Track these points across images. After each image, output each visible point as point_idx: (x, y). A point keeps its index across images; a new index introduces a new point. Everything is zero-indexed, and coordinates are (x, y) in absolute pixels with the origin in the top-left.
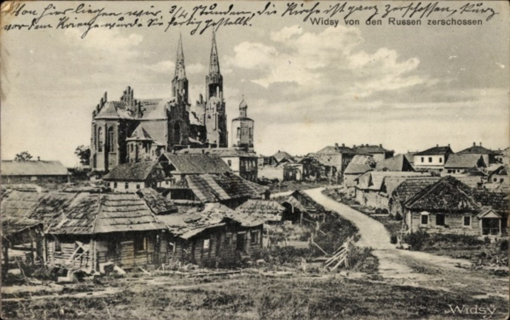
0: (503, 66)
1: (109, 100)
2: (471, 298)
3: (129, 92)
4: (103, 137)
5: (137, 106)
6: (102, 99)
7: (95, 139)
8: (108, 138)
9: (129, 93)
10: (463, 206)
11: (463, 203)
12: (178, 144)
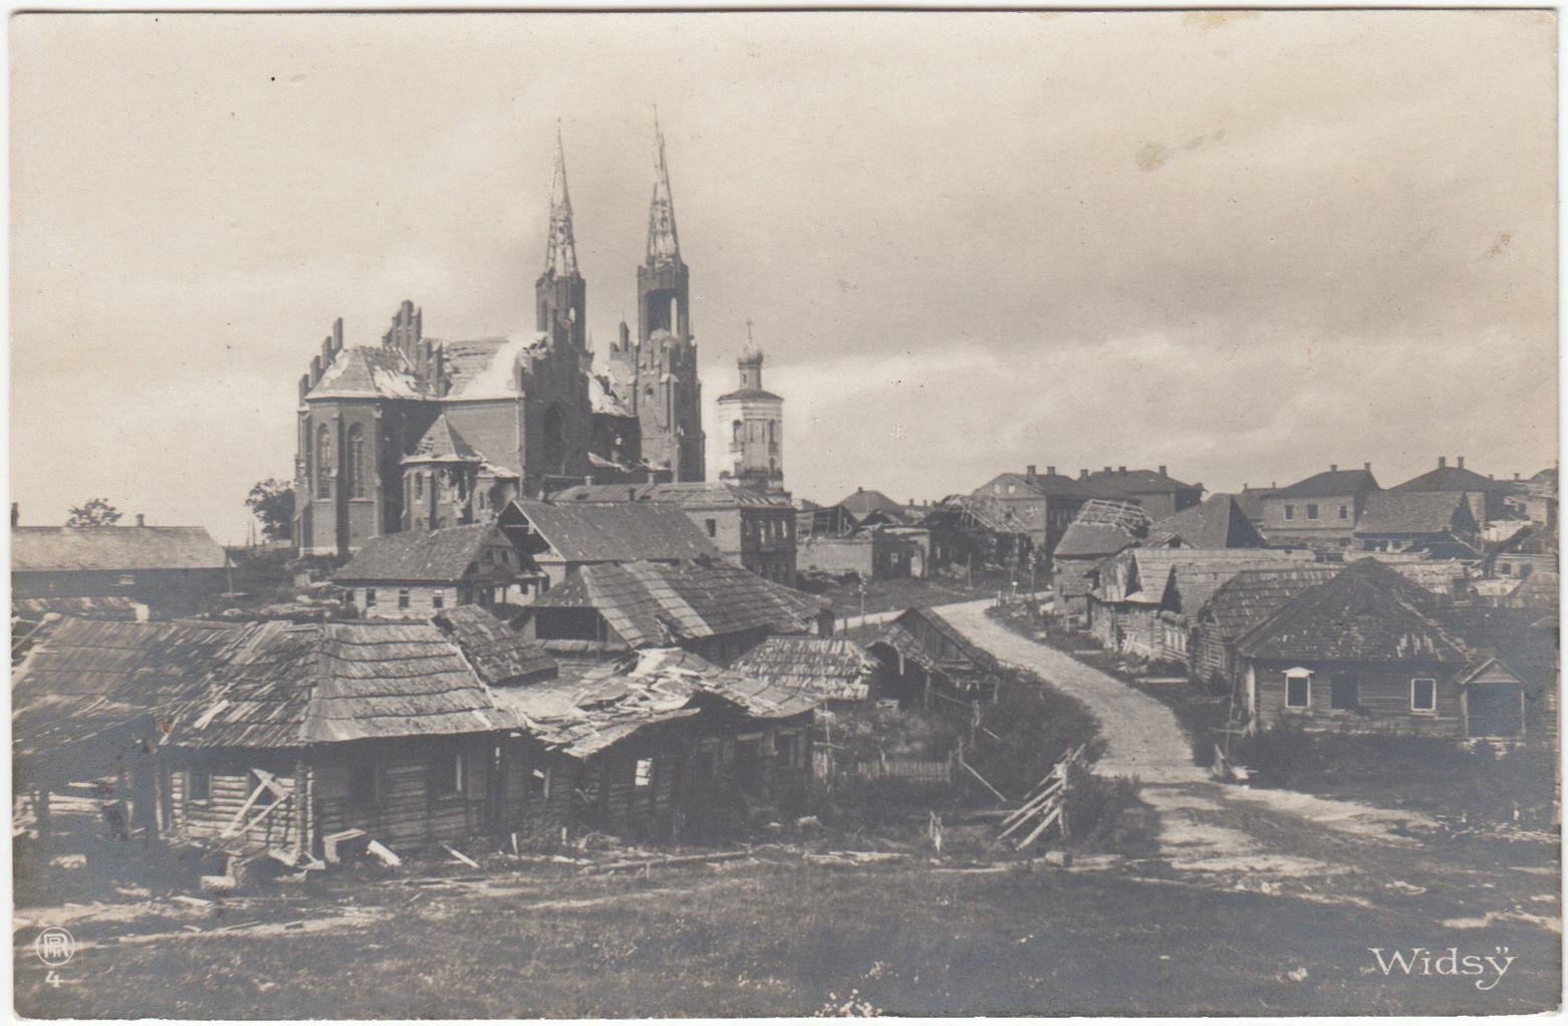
4: (331, 452)
12: (559, 472)
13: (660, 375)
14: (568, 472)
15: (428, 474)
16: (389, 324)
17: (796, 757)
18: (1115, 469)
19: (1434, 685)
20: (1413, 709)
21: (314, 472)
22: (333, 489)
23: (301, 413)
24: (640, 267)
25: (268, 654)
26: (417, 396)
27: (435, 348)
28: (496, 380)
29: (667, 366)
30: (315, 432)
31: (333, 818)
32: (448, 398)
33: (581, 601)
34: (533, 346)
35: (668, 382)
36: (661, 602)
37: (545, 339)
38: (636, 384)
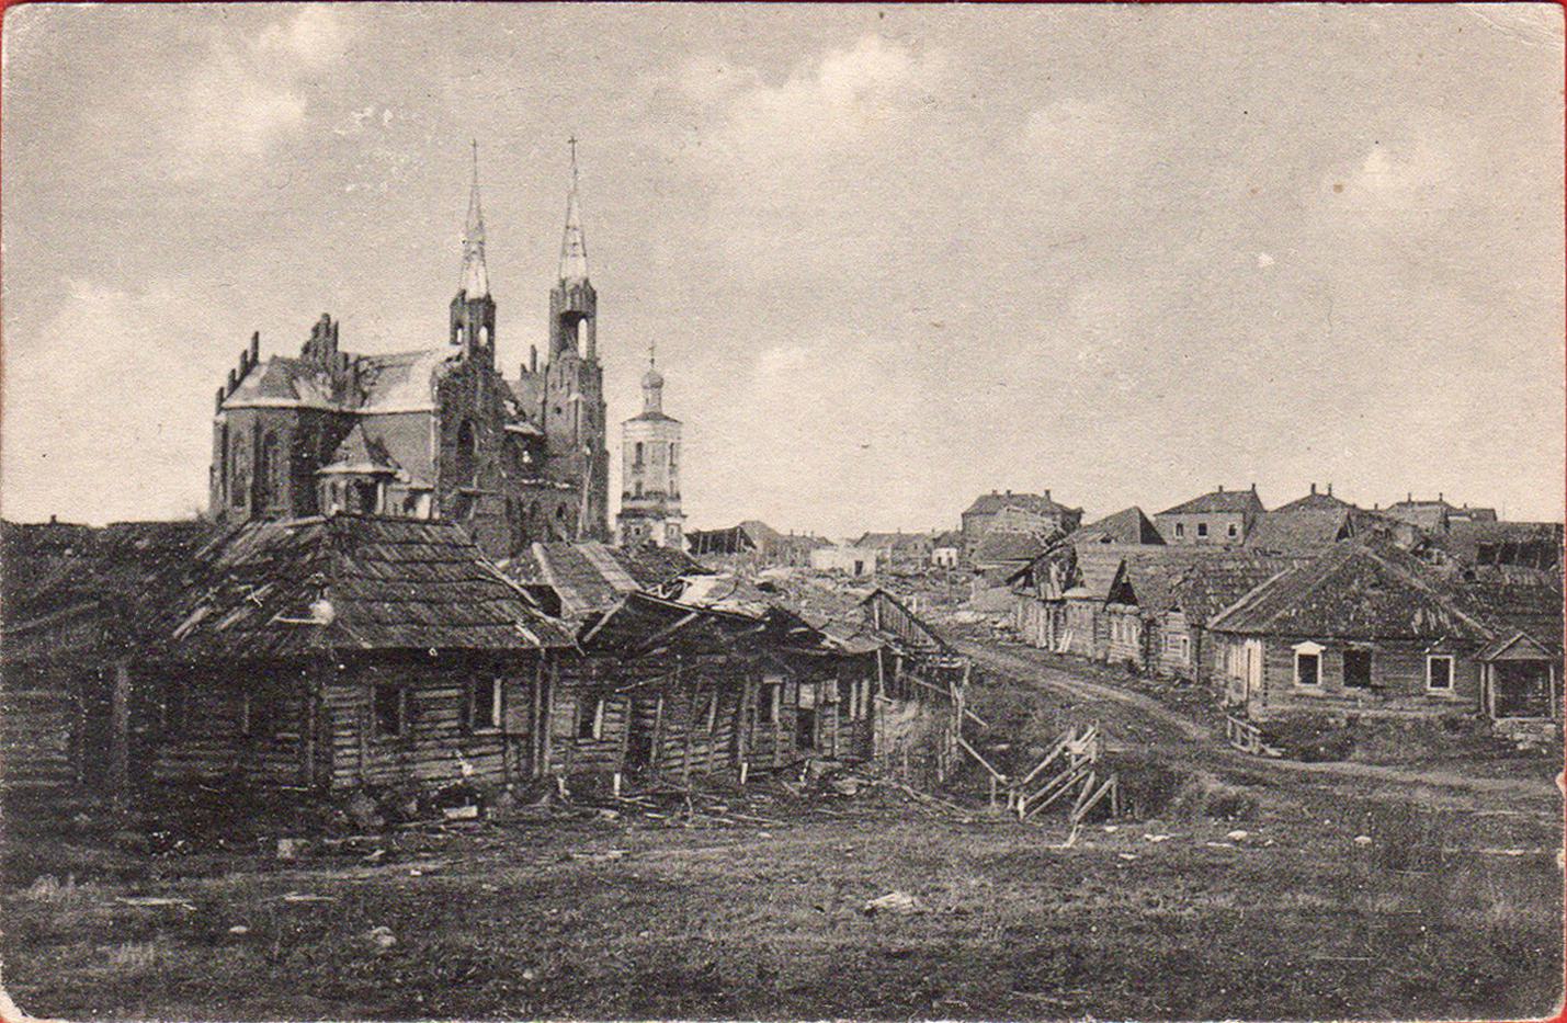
0: (180, 843)
1: (263, 357)
2: (25, 902)
3: (327, 331)
4: (244, 462)
5: (349, 373)
6: (245, 354)
7: (224, 465)
8: (260, 467)
9: (328, 331)
10: (1425, 623)
11: (1424, 614)
12: (471, 485)
13: (569, 395)
14: (480, 485)
15: (342, 484)
16: (309, 336)
17: (859, 706)
18: (1002, 492)
19: (1452, 663)
20: (1429, 688)
21: (230, 480)
22: (248, 499)
23: (216, 424)
24: (552, 291)
25: (264, 554)
26: (334, 407)
27: (352, 360)
28: (411, 396)
29: (576, 384)
30: (230, 440)
31: (348, 751)
32: (363, 410)
33: (534, 579)
34: (449, 360)
35: (577, 402)
36: (614, 584)
37: (461, 353)
38: (544, 402)
